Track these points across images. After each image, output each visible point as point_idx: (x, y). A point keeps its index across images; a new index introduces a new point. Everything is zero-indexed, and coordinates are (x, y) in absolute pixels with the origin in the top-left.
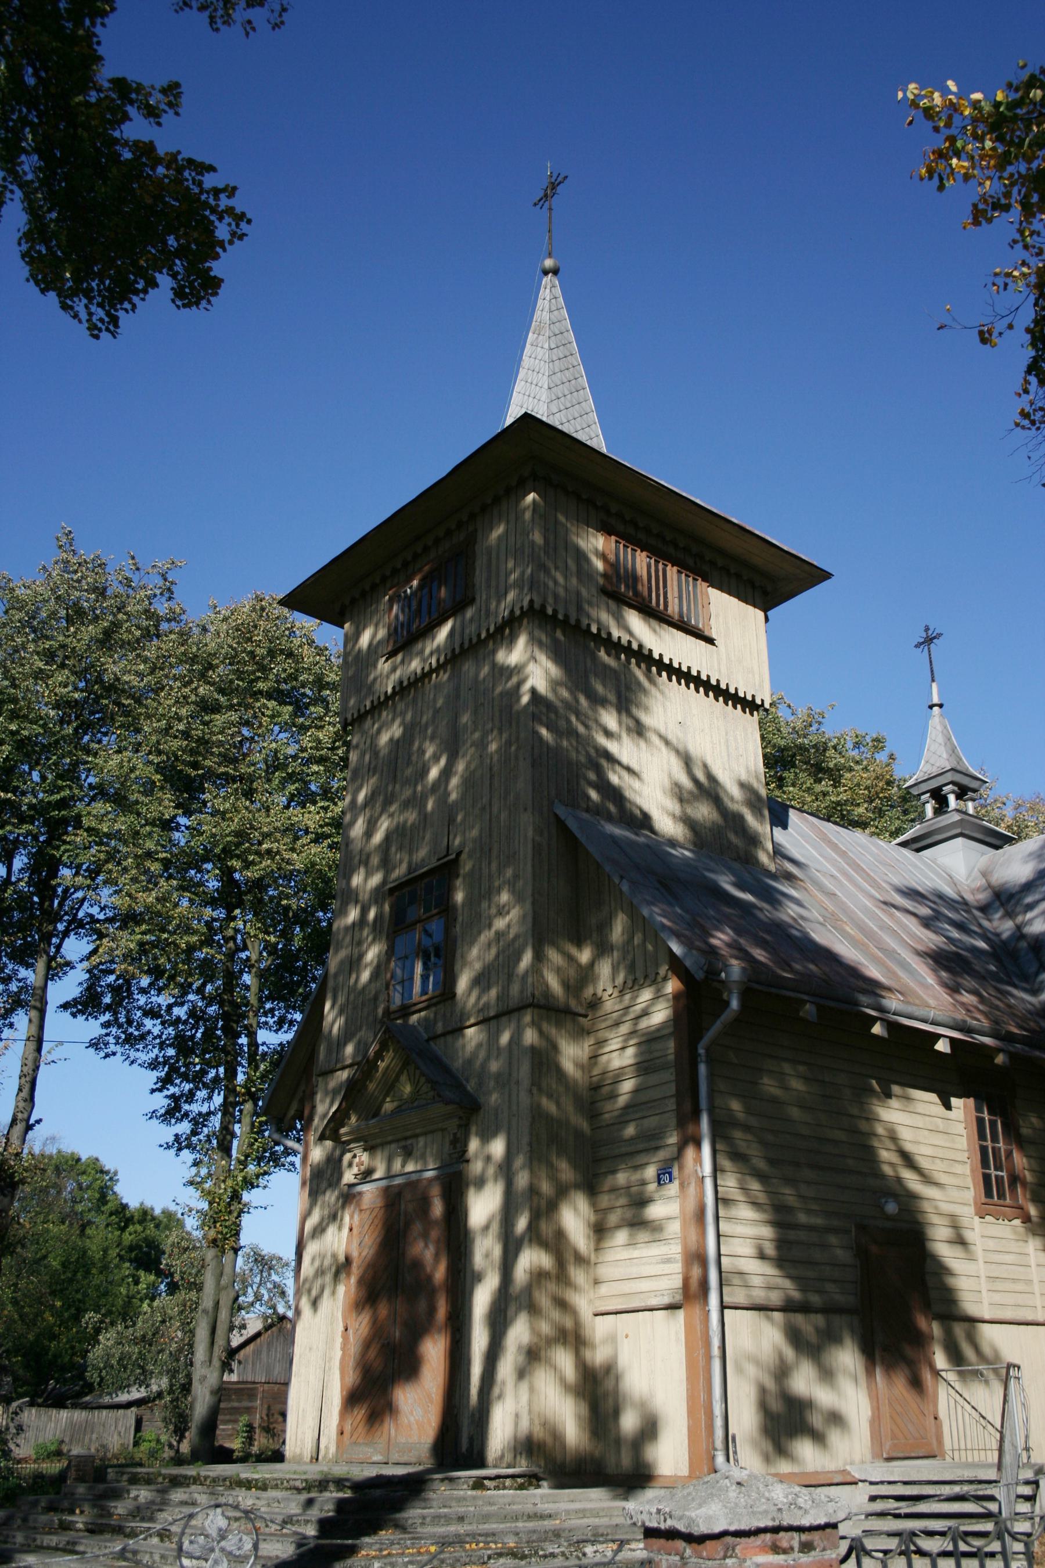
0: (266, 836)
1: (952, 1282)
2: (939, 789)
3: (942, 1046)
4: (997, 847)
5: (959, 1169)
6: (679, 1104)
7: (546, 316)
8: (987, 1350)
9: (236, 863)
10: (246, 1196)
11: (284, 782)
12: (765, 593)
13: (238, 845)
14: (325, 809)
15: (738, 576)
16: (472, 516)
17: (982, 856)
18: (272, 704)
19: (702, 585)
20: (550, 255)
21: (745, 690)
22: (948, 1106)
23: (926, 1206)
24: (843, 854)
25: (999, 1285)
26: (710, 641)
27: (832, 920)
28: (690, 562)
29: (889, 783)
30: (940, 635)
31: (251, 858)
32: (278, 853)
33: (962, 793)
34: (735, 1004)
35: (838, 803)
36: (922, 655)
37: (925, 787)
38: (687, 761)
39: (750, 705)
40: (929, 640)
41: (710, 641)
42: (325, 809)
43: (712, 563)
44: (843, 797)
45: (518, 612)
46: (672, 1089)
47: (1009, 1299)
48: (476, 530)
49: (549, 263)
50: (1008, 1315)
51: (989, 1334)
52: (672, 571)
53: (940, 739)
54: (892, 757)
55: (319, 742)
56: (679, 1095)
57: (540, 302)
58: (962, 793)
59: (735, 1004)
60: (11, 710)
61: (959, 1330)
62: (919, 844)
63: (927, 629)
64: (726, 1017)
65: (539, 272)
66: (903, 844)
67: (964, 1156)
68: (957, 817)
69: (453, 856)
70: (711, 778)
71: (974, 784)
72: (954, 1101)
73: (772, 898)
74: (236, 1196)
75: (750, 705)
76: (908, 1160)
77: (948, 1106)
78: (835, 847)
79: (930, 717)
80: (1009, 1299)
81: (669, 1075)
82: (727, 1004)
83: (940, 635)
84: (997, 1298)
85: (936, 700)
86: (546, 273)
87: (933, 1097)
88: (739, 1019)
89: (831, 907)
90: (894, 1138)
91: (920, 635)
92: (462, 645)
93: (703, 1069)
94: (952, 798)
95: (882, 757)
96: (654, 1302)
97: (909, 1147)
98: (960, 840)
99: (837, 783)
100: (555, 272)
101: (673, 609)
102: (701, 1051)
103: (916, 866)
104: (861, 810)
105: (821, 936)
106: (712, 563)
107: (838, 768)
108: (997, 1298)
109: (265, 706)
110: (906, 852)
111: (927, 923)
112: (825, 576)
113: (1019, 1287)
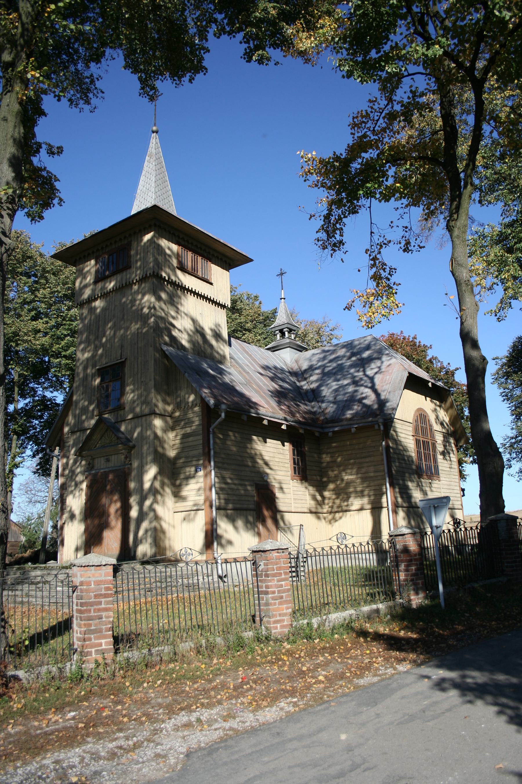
0: (26, 334)
1: (277, 501)
2: (282, 329)
3: (284, 427)
4: (301, 351)
5: (286, 465)
6: (203, 447)
7: (153, 151)
8: (287, 523)
9: (13, 344)
10: (15, 471)
11: (30, 311)
12: (230, 265)
13: (13, 337)
14: (47, 323)
15: (221, 259)
16: (130, 235)
17: (296, 354)
18: (24, 278)
19: (209, 263)
20: (155, 125)
21: (222, 302)
22: (284, 445)
23: (271, 477)
24: (250, 356)
25: (297, 501)
26: (211, 284)
27: (248, 383)
28: (206, 255)
29: (259, 315)
30: (285, 273)
31: (19, 342)
32: (30, 340)
33: (290, 331)
34: (223, 415)
35: (241, 323)
36: (279, 279)
37: (277, 328)
38: (194, 321)
39: (223, 306)
40: (282, 274)
41: (211, 284)
42: (47, 323)
43: (213, 255)
44: (242, 320)
45: (148, 275)
46: (201, 442)
47: (300, 505)
48: (131, 241)
49: (154, 128)
50: (299, 510)
51: (287, 516)
52: (199, 258)
53: (284, 311)
54: (260, 303)
55: (45, 295)
56: (203, 444)
57: (151, 144)
58: (290, 331)
59: (223, 415)
60: (193, 422)
61: (279, 517)
62: (273, 349)
63: (281, 270)
64: (219, 420)
65: (151, 131)
66: (268, 349)
67: (288, 461)
68: (288, 341)
69: (123, 360)
70: (203, 329)
71: (294, 328)
72: (286, 444)
73: (221, 372)
74: (11, 471)
75: (223, 306)
76: (266, 464)
77: (284, 445)
78: (247, 353)
79: (280, 303)
80: (300, 505)
81: (200, 437)
82: (220, 416)
83: (285, 273)
84: (296, 505)
85: (283, 297)
86: (153, 132)
87: (279, 442)
88: (224, 420)
89: (248, 378)
90: (261, 455)
91: (279, 272)
92: (126, 283)
93: (211, 436)
94: (286, 333)
95: (257, 303)
96: (306, 511)
97: (266, 458)
98: (289, 349)
99: (240, 315)
100: (157, 132)
101: (200, 274)
102: (211, 430)
103: (273, 358)
104: (249, 325)
105: (240, 388)
106: (213, 255)
107: (241, 309)
108: (296, 505)
109: (21, 279)
110: (269, 352)
111: (272, 379)
112: (251, 260)
113: (303, 502)
